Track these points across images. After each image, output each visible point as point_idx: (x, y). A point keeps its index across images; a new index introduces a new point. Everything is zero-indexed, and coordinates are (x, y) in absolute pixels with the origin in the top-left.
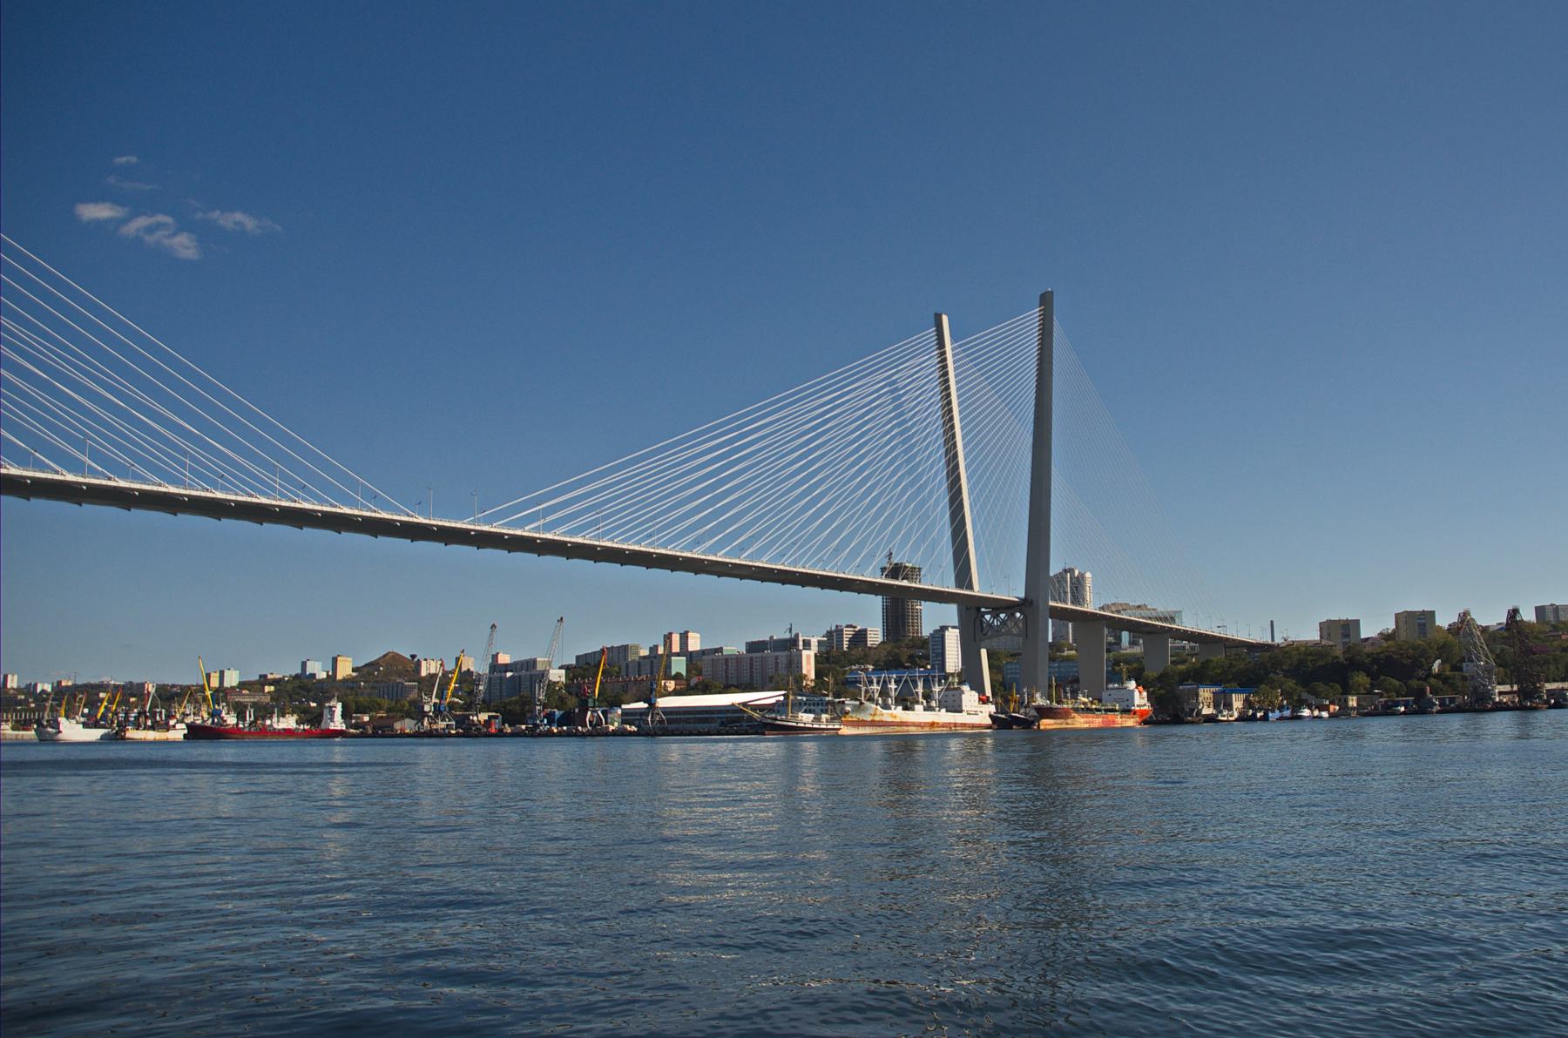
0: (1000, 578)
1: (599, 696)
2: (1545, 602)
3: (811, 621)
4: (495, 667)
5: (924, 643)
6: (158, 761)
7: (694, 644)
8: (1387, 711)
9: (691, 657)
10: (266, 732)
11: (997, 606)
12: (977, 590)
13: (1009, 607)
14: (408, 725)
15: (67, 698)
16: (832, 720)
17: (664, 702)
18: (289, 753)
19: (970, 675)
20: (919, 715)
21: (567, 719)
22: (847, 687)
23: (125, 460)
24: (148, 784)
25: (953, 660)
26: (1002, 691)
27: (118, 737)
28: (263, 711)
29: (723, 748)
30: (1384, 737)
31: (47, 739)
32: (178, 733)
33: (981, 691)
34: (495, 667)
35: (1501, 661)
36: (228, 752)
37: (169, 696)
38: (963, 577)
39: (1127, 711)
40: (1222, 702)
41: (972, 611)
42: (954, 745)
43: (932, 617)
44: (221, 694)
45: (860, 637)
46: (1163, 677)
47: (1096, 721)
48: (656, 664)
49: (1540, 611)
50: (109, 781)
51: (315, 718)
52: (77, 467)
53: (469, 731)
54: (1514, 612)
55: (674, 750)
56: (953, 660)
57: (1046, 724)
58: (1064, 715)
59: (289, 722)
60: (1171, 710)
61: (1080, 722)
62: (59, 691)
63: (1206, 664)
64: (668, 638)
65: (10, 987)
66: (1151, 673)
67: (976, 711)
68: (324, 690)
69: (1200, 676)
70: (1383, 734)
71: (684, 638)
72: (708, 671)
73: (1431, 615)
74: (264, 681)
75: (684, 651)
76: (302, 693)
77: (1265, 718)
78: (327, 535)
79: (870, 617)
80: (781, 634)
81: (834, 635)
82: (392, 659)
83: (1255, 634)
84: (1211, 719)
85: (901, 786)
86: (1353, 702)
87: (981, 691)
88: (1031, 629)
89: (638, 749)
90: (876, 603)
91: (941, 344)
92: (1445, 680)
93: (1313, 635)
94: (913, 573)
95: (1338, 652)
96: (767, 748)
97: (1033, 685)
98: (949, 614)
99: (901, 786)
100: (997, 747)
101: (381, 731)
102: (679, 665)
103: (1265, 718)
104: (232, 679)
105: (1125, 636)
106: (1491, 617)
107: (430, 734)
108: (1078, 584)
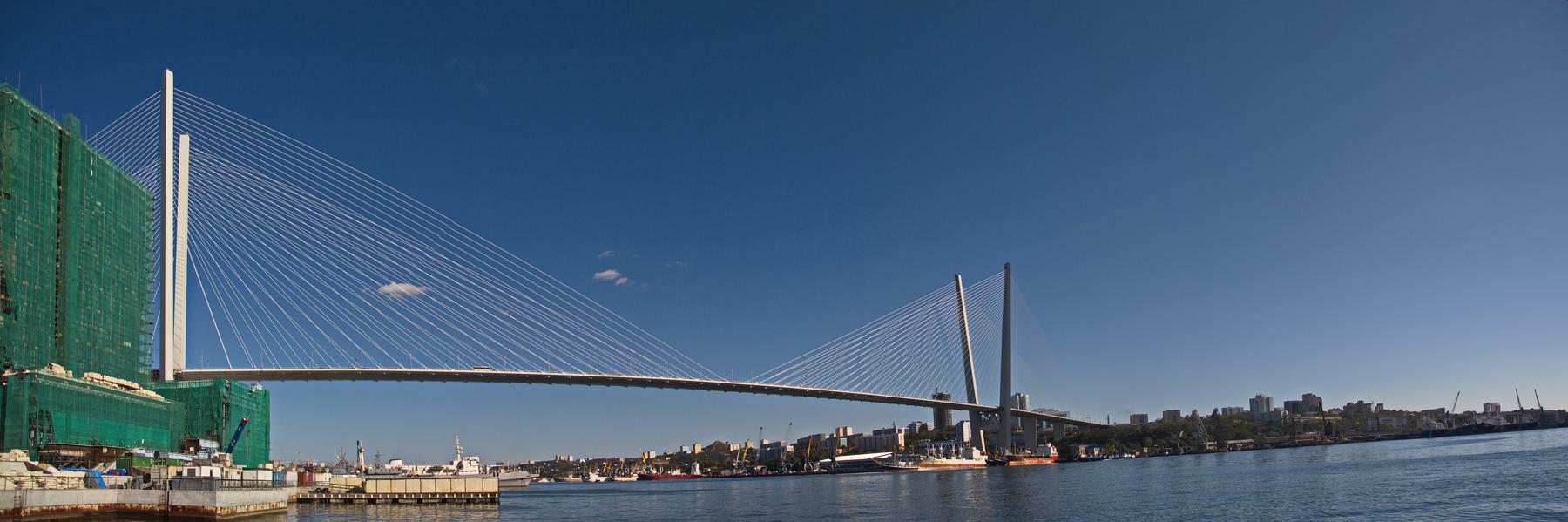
0: (988, 398)
1: (812, 453)
3: (901, 420)
4: (762, 446)
6: (626, 490)
7: (850, 432)
8: (1161, 454)
9: (849, 438)
11: (987, 411)
12: (978, 404)
13: (993, 411)
14: (727, 472)
15: (593, 464)
17: (838, 459)
19: (975, 442)
20: (954, 461)
22: (921, 450)
24: (622, 499)
25: (967, 436)
26: (990, 450)
27: (611, 480)
28: (667, 468)
29: (866, 478)
31: (586, 481)
32: (634, 478)
34: (762, 446)
36: (653, 486)
37: (630, 463)
38: (971, 398)
39: (1048, 457)
41: (976, 414)
42: (969, 474)
44: (649, 461)
45: (924, 427)
47: (1034, 462)
48: (833, 442)
50: (608, 498)
51: (688, 470)
52: (588, 371)
53: (753, 474)
55: (844, 479)
56: (967, 436)
57: (1012, 463)
58: (1020, 459)
59: (678, 472)
60: (1067, 456)
61: (1027, 462)
62: (588, 462)
66: (1057, 440)
67: (979, 458)
68: (691, 458)
69: (1080, 440)
70: (1157, 463)
72: (856, 444)
73: (1268, 400)
74: (666, 455)
75: (845, 435)
76: (681, 460)
78: (721, 393)
79: (927, 417)
81: (913, 426)
82: (718, 445)
89: (828, 480)
90: (931, 410)
94: (947, 397)
96: (886, 477)
97: (1005, 446)
98: (966, 415)
100: (989, 474)
101: (716, 475)
102: (844, 442)
104: (653, 455)
106: (1205, 412)
107: (737, 476)
108: (1023, 400)
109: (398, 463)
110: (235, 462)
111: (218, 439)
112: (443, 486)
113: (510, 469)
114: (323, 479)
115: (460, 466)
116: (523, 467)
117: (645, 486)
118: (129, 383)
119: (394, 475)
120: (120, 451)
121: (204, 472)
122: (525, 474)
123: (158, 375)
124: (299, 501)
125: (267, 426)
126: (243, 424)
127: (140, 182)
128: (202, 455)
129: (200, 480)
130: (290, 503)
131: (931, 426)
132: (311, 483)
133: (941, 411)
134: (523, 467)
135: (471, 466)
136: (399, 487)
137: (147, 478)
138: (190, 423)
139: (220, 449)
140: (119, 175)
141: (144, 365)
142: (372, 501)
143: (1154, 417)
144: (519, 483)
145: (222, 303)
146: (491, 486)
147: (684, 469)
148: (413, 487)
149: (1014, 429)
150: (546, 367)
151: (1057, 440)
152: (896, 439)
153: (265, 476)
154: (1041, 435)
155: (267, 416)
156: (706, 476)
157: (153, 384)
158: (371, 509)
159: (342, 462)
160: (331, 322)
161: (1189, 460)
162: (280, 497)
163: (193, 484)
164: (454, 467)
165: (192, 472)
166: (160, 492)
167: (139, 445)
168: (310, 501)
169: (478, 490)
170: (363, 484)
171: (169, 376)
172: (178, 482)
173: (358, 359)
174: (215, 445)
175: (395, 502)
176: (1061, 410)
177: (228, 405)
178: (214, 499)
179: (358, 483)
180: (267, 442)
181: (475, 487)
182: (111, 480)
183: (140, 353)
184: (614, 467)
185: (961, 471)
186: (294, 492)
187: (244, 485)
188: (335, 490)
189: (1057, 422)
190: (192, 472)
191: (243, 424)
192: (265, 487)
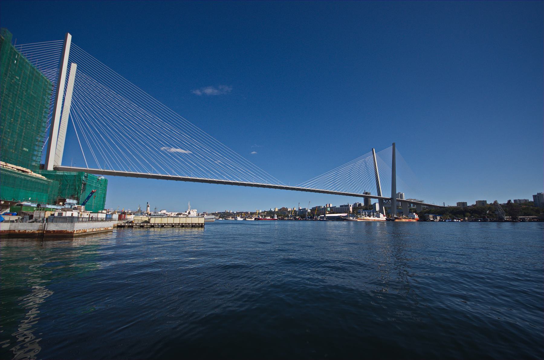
0: (387, 194)
1: (316, 214)
2: (517, 199)
3: (351, 202)
4: (299, 209)
5: (372, 206)
7: (331, 206)
8: (476, 221)
10: (266, 219)
11: (386, 199)
12: (382, 196)
13: (388, 199)
14: (286, 218)
15: (239, 214)
16: (53, 215)
17: (327, 215)
18: (268, 223)
19: (381, 211)
20: (372, 218)
21: (311, 218)
22: (359, 213)
23: (217, 176)
25: (378, 208)
26: (387, 214)
27: (245, 220)
28: (265, 216)
30: (475, 226)
31: (236, 220)
32: (253, 219)
33: (383, 214)
34: (299, 209)
35: (505, 211)
36: (260, 222)
37: (252, 214)
38: (379, 194)
39: (414, 219)
40: (435, 217)
43: (373, 201)
44: (259, 213)
45: (360, 205)
46: (421, 212)
47: (407, 220)
48: (325, 209)
49: (514, 200)
51: (273, 217)
52: (239, 180)
53: (296, 219)
54: (509, 201)
56: (378, 208)
57: (397, 220)
58: (400, 219)
59: (269, 218)
60: (423, 218)
61: (404, 220)
63: (430, 210)
64: (327, 205)
65: (4, 344)
66: (418, 212)
67: (383, 218)
69: (429, 212)
71: (329, 205)
72: (334, 210)
74: (265, 211)
76: (271, 213)
77: (445, 221)
79: (361, 201)
80: (346, 204)
81: (356, 204)
82: (283, 208)
83: (441, 205)
84: (432, 221)
85: (369, 232)
86: (466, 219)
87: (383, 214)
88: (392, 203)
91: (373, 154)
92: (490, 215)
93: (456, 205)
94: (369, 194)
95: (462, 208)
96: (345, 223)
97: (394, 213)
98: (377, 201)
99: (369, 232)
101: (283, 219)
102: (329, 209)
103: (445, 221)
104: (260, 211)
105: (412, 205)
109: (164, 211)
110: (86, 210)
111: (77, 199)
112: (183, 221)
113: (208, 215)
114: (131, 218)
115: (189, 213)
116: (213, 214)
117: (257, 222)
118: (24, 169)
119: (162, 216)
120: (13, 203)
121: (69, 214)
122: (213, 217)
123: (43, 167)
124: (119, 227)
125: (105, 194)
126: (92, 193)
127: (47, 75)
128: (67, 206)
129: (66, 218)
130: (114, 227)
131: (363, 204)
132: (124, 219)
133: (367, 199)
134: (213, 214)
135: (194, 213)
136: (165, 221)
137: (31, 217)
138: (61, 191)
139: (78, 204)
140: (33, 68)
141: (35, 161)
142: (152, 226)
143: (471, 203)
144: (211, 220)
145: (85, 136)
146: (202, 221)
147: (271, 217)
148: (171, 221)
149: (398, 207)
150: (224, 179)
151: (418, 212)
152: (349, 209)
153: (102, 216)
154: (410, 210)
155: (106, 190)
156: (279, 220)
157: (40, 171)
158: (152, 229)
159: (139, 211)
160: (139, 154)
161: (493, 226)
162: (110, 225)
163: (61, 220)
164: (187, 213)
165: (60, 214)
166: (39, 224)
167: (27, 200)
168: (124, 226)
169: (196, 222)
170: (149, 219)
171: (50, 168)
172: (52, 219)
173: (150, 170)
174: (75, 202)
175: (162, 226)
176: (419, 200)
177: (85, 184)
178: (74, 226)
179: (147, 219)
180: (104, 201)
181: (196, 221)
182: (7, 218)
183: (34, 155)
184: (246, 215)
185: (375, 222)
186: (116, 223)
187: (91, 220)
188: (136, 222)
189: (418, 204)
190: (60, 214)
191: (92, 193)
192: (102, 220)
